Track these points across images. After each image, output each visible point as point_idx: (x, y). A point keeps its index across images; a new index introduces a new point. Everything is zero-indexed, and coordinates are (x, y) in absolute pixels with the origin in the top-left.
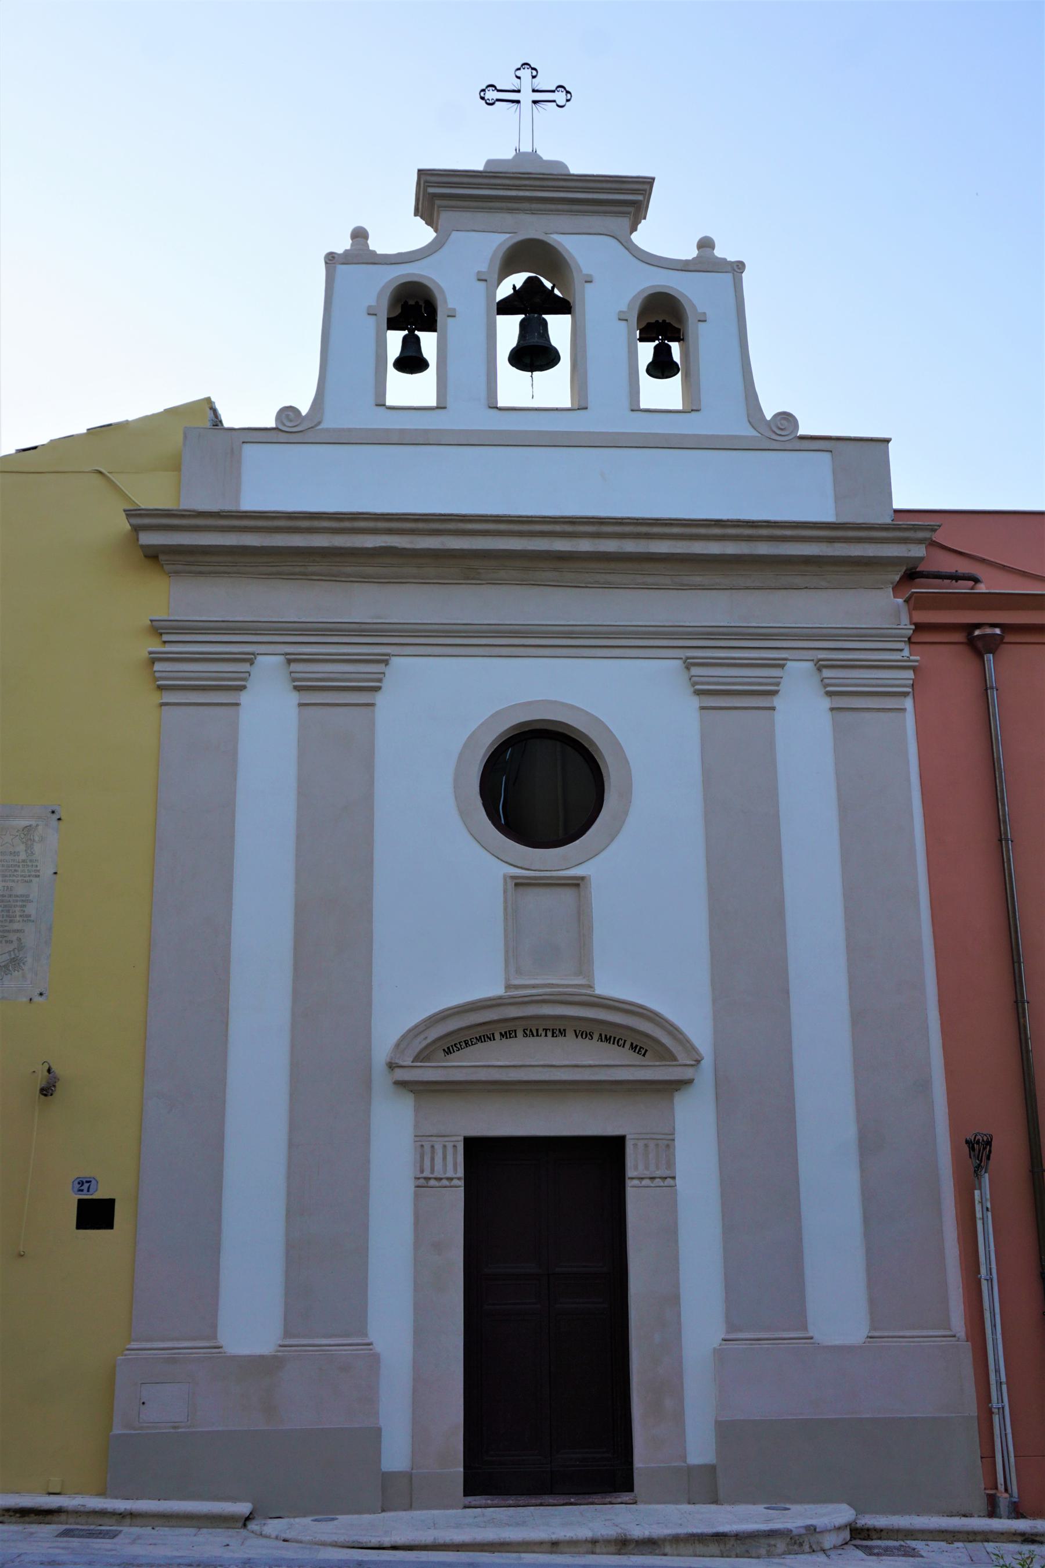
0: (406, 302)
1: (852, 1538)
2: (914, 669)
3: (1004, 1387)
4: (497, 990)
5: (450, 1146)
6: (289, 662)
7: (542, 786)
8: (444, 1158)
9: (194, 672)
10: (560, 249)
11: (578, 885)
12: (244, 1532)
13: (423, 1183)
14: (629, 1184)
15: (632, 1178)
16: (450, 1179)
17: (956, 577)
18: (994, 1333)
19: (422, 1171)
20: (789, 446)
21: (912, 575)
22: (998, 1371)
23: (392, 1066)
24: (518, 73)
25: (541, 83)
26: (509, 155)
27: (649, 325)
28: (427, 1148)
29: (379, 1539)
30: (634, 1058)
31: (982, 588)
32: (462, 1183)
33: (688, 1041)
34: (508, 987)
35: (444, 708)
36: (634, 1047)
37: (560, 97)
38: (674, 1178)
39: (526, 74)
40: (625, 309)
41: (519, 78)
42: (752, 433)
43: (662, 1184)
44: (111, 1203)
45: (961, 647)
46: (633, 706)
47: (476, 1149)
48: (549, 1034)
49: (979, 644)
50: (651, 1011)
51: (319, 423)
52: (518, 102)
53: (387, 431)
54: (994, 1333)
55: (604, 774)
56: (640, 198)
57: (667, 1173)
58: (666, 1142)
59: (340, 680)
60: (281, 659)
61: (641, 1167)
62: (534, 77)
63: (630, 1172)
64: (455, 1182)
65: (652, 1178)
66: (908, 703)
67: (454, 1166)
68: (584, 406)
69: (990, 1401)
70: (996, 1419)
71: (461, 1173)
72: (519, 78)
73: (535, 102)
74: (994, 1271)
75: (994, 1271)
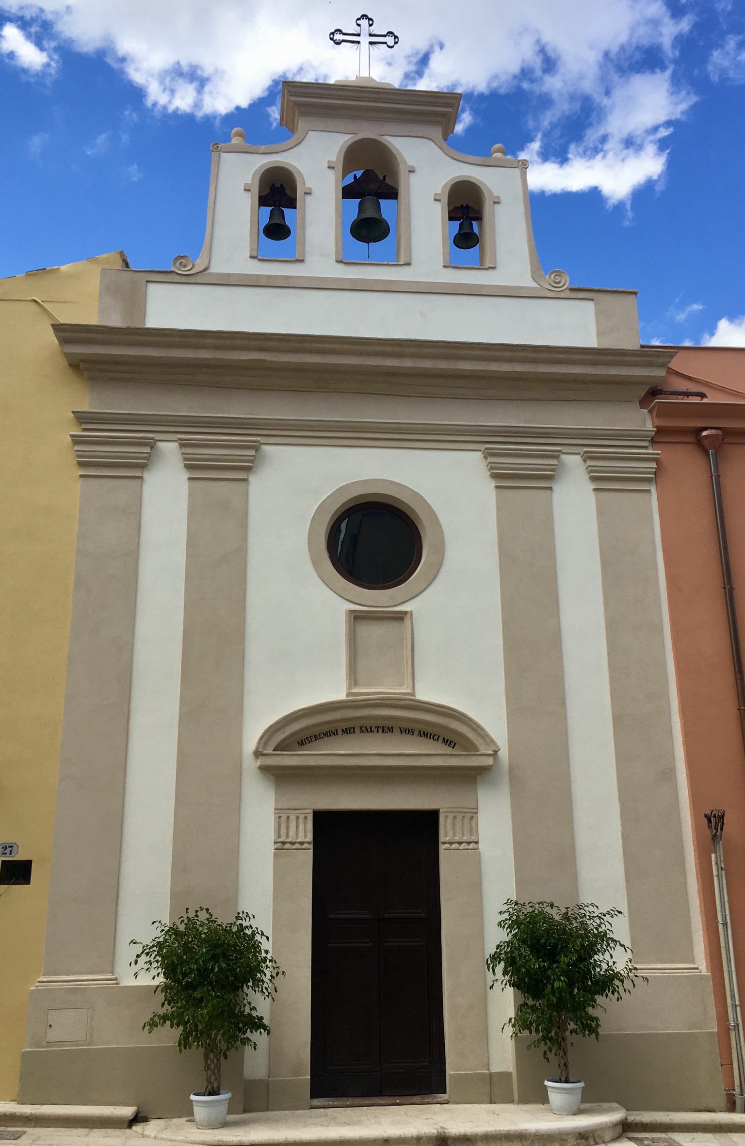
0: (273, 185)
1: (624, 1131)
2: (657, 461)
3: (738, 1009)
4: (340, 694)
5: (302, 817)
6: (182, 446)
7: (375, 543)
8: (297, 827)
9: (110, 454)
10: (390, 146)
11: (402, 619)
12: (128, 1131)
13: (281, 846)
14: (442, 847)
15: (444, 843)
16: (302, 843)
17: (688, 394)
18: (729, 966)
19: (279, 837)
20: (562, 295)
21: (654, 392)
22: (733, 996)
23: (257, 754)
24: (359, 22)
25: (375, 30)
26: (354, 78)
27: (456, 208)
28: (284, 819)
29: (239, 1138)
30: (449, 750)
31: (705, 401)
32: (311, 846)
33: (488, 736)
34: (348, 695)
35: (301, 484)
36: (446, 741)
37: (390, 40)
38: (477, 843)
39: (364, 23)
40: (439, 192)
41: (359, 25)
42: (535, 285)
43: (467, 847)
44: (29, 863)
45: (689, 446)
46: (448, 486)
47: (326, 823)
48: (380, 730)
49: (706, 443)
50: (460, 713)
51: (206, 269)
52: (358, 42)
53: (259, 276)
54: (729, 966)
55: (401, 508)
56: (451, 110)
57: (473, 838)
58: (471, 815)
59: (221, 464)
60: (176, 445)
61: (450, 834)
62: (370, 25)
63: (442, 838)
64: (305, 846)
65: (460, 843)
66: (653, 489)
67: (305, 832)
68: (408, 261)
69: (728, 1020)
70: (733, 1034)
71: (310, 837)
72: (359, 25)
73: (371, 43)
74: (728, 917)
75: (728, 917)
